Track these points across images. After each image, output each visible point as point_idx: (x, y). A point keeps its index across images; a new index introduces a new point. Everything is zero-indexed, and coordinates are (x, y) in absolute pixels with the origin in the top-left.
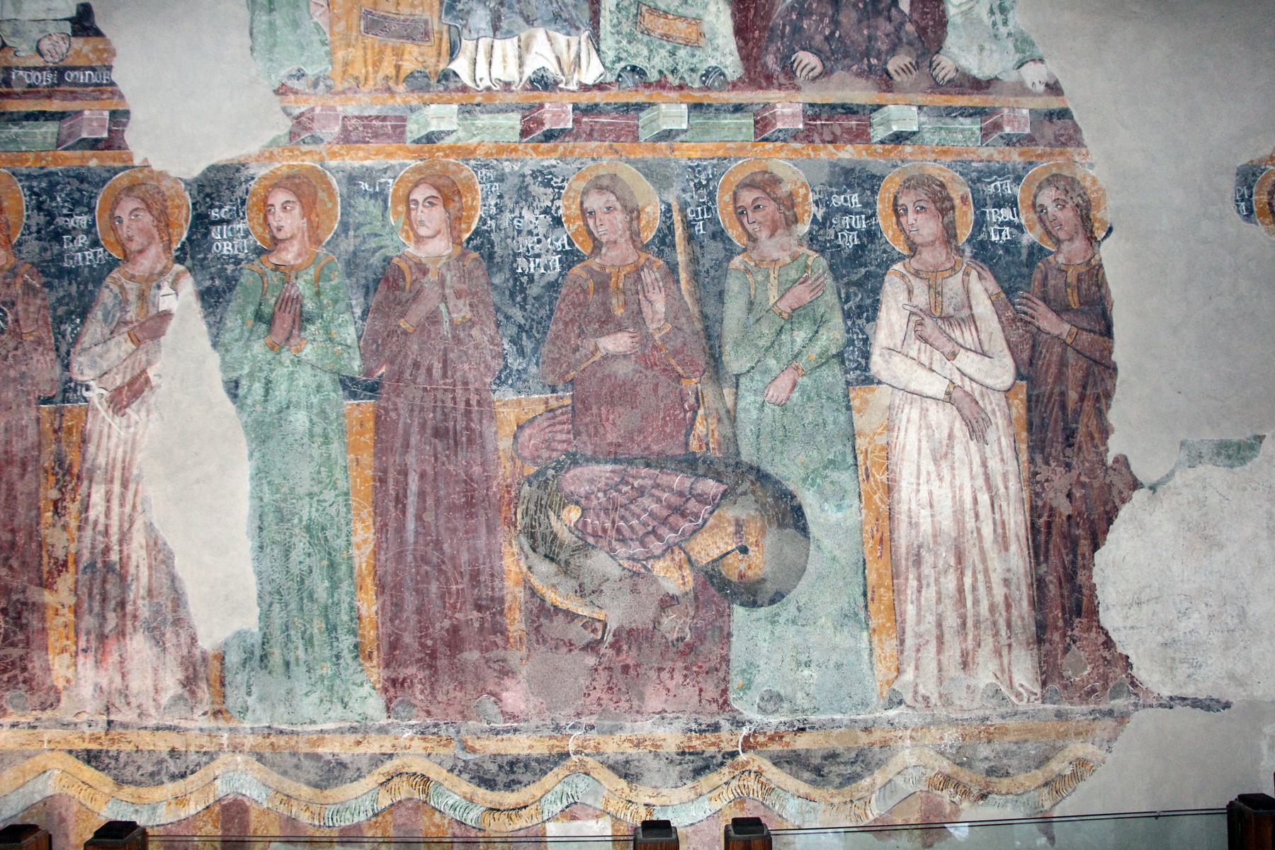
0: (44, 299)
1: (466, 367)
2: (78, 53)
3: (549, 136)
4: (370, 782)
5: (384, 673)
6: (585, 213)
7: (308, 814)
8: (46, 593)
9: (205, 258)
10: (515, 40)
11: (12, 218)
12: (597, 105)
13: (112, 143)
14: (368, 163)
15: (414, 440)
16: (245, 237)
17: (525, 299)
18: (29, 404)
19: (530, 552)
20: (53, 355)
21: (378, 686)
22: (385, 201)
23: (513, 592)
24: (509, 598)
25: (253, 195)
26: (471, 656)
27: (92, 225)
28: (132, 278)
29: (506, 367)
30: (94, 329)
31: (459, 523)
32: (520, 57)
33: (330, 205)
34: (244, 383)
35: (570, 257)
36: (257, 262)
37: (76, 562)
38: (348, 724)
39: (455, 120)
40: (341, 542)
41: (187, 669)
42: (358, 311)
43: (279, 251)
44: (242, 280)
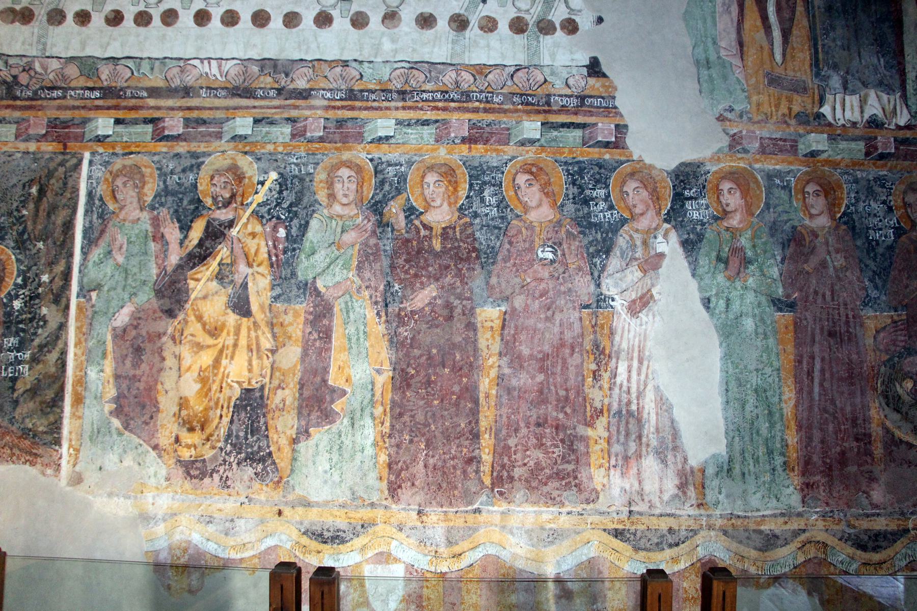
0: (580, 242)
1: (845, 295)
2: (593, 87)
3: (882, 157)
4: (796, 544)
5: (802, 480)
6: (906, 205)
7: (754, 567)
8: (589, 429)
9: (683, 221)
10: (858, 96)
11: (557, 189)
12: (908, 139)
13: (618, 144)
14: (777, 167)
15: (817, 339)
16: (707, 209)
17: (875, 255)
18: (574, 309)
19: (886, 407)
20: (589, 277)
21: (798, 487)
22: (790, 191)
23: (876, 430)
24: (874, 434)
25: (710, 182)
26: (852, 469)
27: (608, 196)
28: (637, 231)
29: (868, 295)
30: (614, 263)
31: (845, 388)
32: (861, 107)
33: (758, 192)
34: (713, 299)
35: (899, 232)
36: (715, 225)
37: (609, 410)
38: (779, 511)
39: (826, 144)
40: (776, 399)
41: (681, 478)
42: (779, 258)
43: (728, 219)
44: (707, 235)
